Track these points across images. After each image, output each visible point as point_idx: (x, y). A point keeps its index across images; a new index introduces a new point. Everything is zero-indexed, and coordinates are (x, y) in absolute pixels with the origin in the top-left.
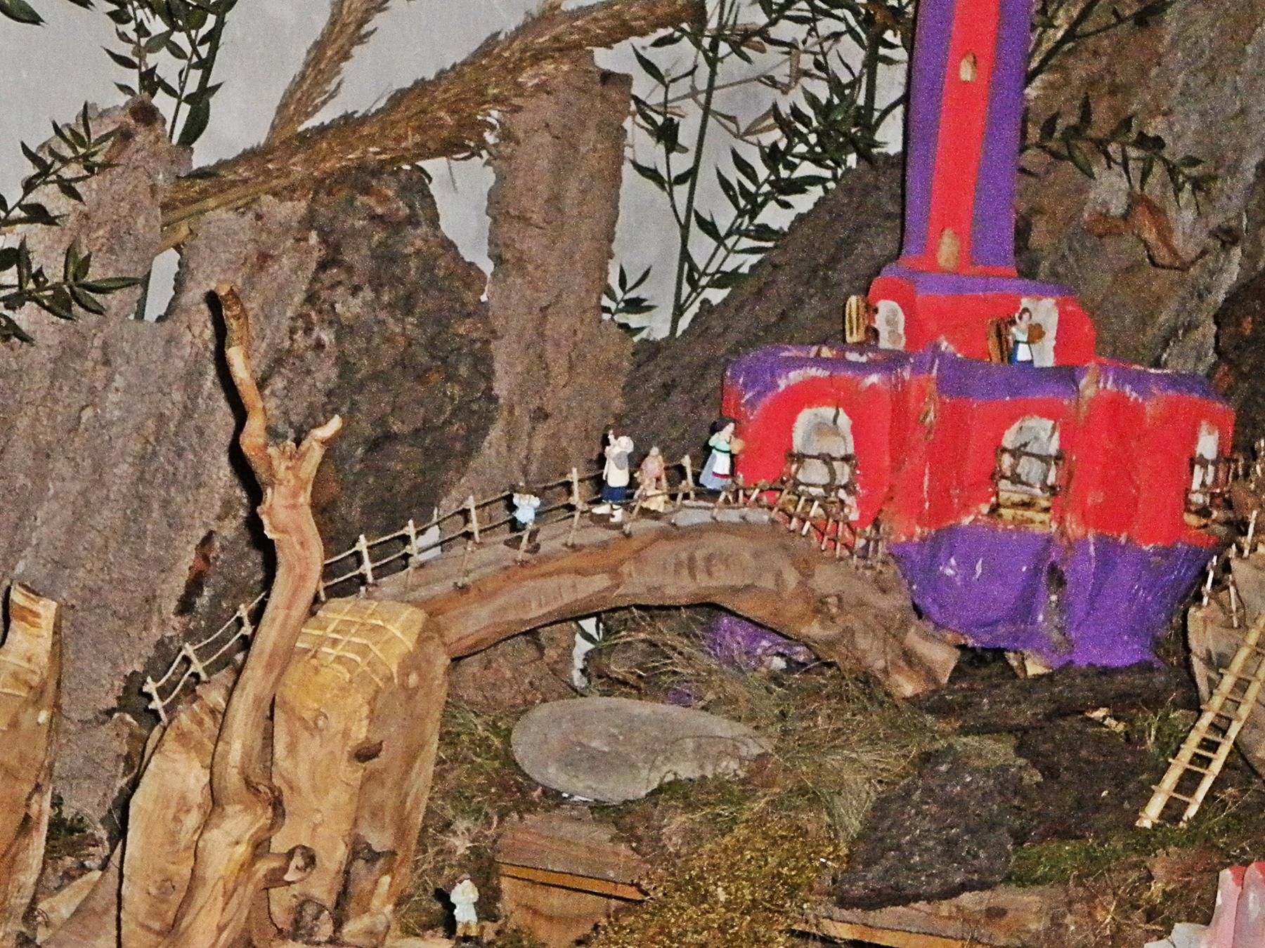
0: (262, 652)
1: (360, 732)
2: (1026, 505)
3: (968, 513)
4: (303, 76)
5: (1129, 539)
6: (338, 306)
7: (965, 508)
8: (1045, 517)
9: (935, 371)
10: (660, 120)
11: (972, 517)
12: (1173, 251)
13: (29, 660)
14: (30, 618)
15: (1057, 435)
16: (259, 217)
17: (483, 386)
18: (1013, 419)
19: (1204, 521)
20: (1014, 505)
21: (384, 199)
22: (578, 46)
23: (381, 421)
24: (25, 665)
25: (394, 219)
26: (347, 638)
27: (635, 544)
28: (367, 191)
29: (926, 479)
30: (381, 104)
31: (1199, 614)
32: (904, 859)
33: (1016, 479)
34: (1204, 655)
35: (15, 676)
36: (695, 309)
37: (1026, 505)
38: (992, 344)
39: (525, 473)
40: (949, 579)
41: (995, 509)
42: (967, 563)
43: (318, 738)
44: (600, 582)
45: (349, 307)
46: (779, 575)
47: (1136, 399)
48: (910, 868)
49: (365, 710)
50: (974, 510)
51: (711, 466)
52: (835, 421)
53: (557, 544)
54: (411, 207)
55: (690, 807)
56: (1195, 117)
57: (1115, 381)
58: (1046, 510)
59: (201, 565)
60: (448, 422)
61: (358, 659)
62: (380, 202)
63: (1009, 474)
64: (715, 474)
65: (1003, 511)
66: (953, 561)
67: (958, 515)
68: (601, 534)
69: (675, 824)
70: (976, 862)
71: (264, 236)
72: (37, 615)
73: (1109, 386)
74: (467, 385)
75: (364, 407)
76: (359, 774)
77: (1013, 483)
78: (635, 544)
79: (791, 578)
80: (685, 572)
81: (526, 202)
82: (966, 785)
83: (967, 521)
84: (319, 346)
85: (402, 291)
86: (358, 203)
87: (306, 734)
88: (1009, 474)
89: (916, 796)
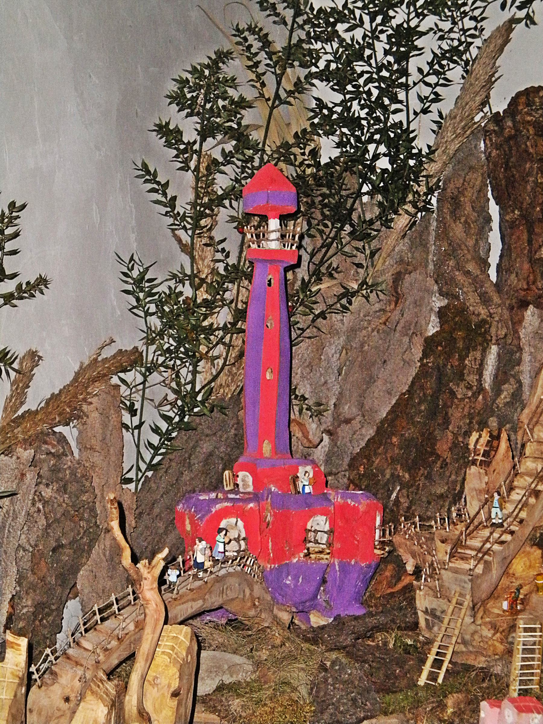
0: (144, 654)
1: (175, 684)
2: (321, 552)
3: (295, 558)
4: (12, 396)
5: (356, 562)
6: (42, 493)
7: (293, 555)
8: (328, 556)
9: (269, 500)
10: (128, 403)
11: (297, 559)
12: (310, 442)
13: (17, 666)
14: (16, 647)
15: (328, 522)
16: (18, 458)
17: (94, 521)
18: (310, 517)
19: (382, 552)
20: (317, 553)
21: (54, 446)
22: (105, 375)
23: (57, 540)
24: (15, 668)
25: (58, 454)
26: (163, 644)
27: (209, 585)
28: (46, 443)
29: (270, 544)
30: (43, 405)
31: (421, 593)
32: (337, 708)
33: (316, 542)
34: (424, 609)
35: (12, 673)
36: (143, 480)
37: (321, 552)
38: (292, 487)
39: (105, 555)
40: (288, 586)
41: (307, 555)
42: (296, 578)
43: (156, 689)
44: (200, 602)
45: (47, 493)
46: (244, 592)
47: (354, 505)
48: (342, 712)
49: (178, 674)
50: (297, 556)
51: (217, 548)
52: (236, 524)
53: (184, 590)
54: (63, 447)
55: (239, 696)
56: (308, 386)
57: (341, 498)
58: (328, 554)
59: (11, 610)
60: (81, 538)
61: (171, 652)
62: (53, 448)
63: (313, 540)
64: (219, 552)
65: (311, 555)
66: (290, 578)
67: (289, 559)
68: (198, 583)
69: (236, 704)
70: (367, 707)
71: (21, 465)
72: (19, 645)
73: (339, 500)
74: (88, 521)
75: (52, 534)
76: (176, 703)
77: (315, 543)
78: (209, 585)
79: (248, 592)
80: (221, 595)
81: (93, 442)
82: (349, 675)
83: (295, 561)
84: (39, 511)
85: (61, 484)
86: (43, 449)
87: (151, 687)
88: (313, 540)
89: (330, 681)
